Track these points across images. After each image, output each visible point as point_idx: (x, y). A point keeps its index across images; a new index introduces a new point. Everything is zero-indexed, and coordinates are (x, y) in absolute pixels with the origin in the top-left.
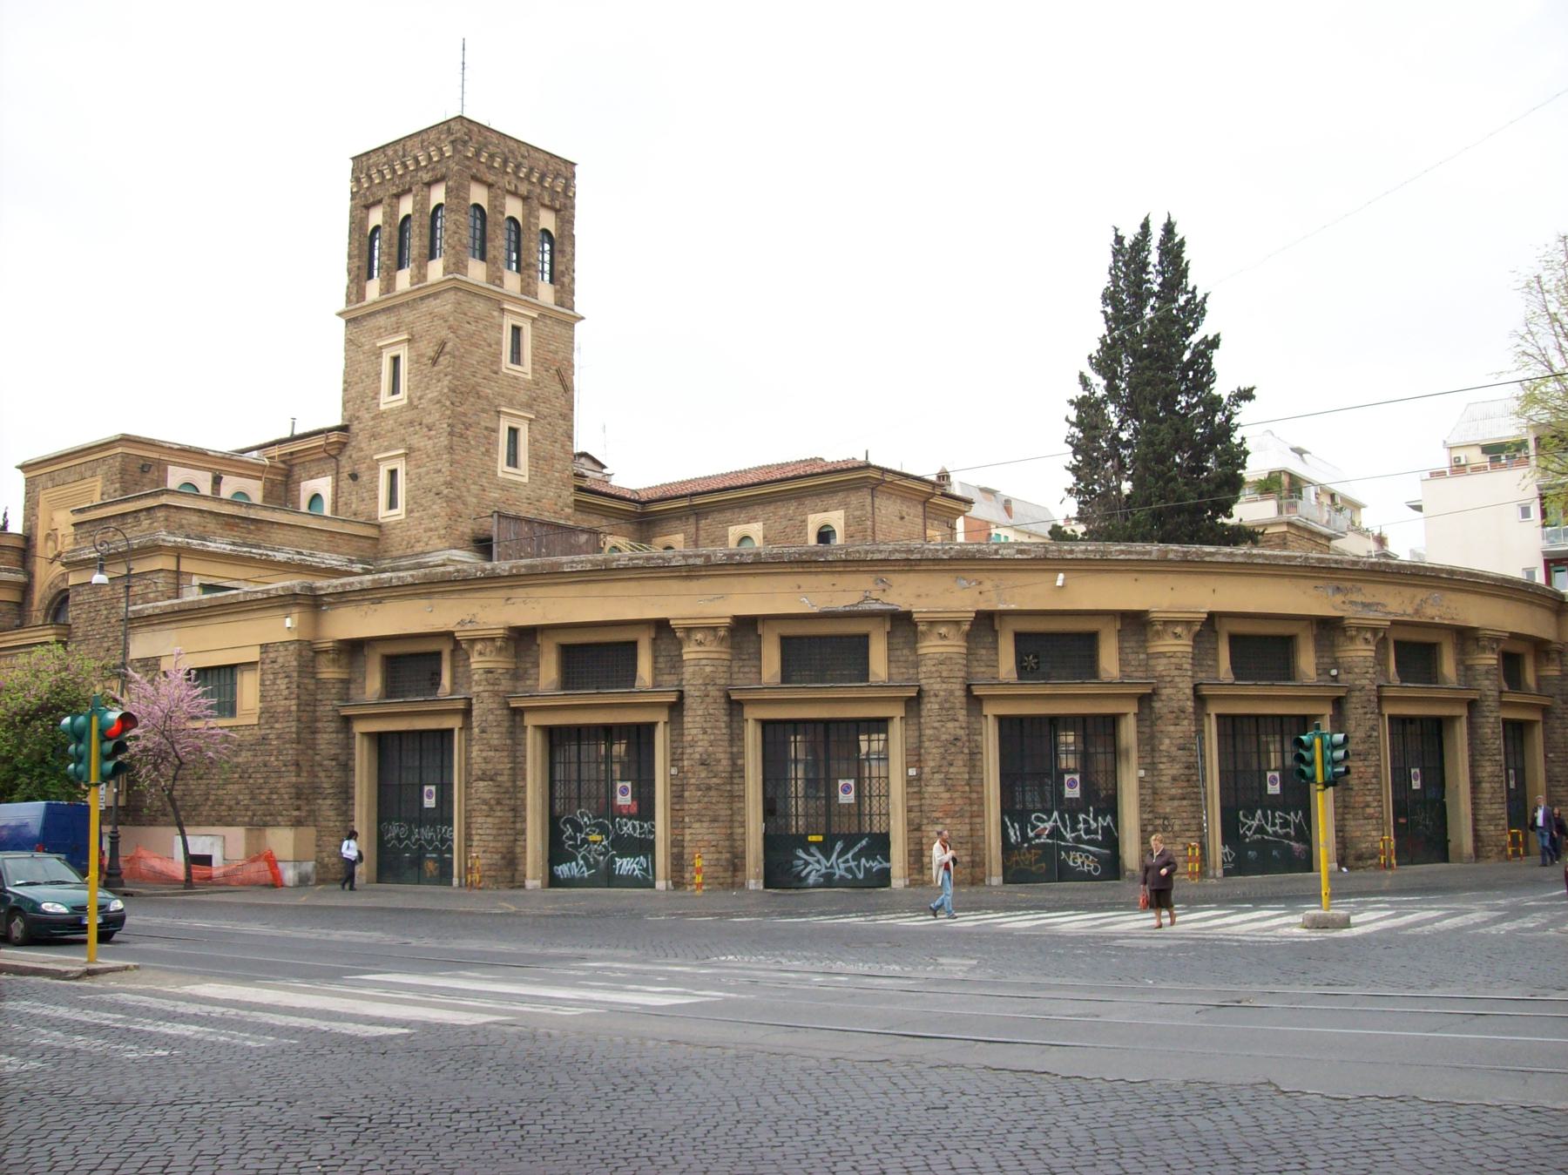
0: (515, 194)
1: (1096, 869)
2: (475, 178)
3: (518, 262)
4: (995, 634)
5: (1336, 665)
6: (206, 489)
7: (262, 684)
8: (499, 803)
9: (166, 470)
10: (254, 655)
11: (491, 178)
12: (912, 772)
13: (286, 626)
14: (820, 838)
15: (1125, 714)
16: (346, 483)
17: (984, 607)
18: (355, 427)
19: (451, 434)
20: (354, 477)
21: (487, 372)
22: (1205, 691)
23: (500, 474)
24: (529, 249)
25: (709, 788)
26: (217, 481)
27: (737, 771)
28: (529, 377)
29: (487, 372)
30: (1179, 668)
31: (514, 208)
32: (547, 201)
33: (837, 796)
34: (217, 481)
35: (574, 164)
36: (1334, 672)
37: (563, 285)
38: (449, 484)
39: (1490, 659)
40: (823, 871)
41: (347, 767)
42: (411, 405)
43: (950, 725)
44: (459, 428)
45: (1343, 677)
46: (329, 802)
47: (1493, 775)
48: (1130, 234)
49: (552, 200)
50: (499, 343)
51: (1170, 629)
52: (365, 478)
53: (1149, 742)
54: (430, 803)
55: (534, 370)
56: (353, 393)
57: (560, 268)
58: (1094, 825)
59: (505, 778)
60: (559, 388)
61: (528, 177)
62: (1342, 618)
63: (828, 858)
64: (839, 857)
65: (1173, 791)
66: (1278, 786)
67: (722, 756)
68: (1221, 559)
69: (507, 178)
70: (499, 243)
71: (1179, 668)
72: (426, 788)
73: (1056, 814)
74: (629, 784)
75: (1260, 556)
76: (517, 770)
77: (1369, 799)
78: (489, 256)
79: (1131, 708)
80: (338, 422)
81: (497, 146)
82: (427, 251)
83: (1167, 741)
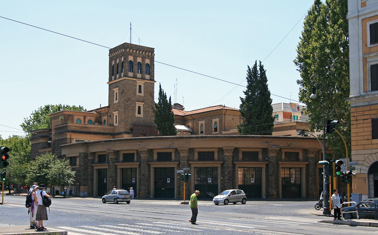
3: (141, 71)
7: (79, 159)
8: (113, 182)
10: (78, 155)
12: (178, 177)
13: (82, 150)
16: (109, 118)
18: (110, 107)
19: (125, 109)
20: (110, 116)
22: (285, 169)
23: (136, 116)
24: (143, 68)
25: (144, 179)
27: (149, 176)
30: (229, 158)
31: (139, 60)
35: (152, 50)
38: (125, 119)
39: (152, 160)
41: (93, 175)
42: (119, 103)
44: (126, 107)
45: (269, 160)
46: (90, 181)
48: (251, 67)
50: (136, 89)
52: (112, 117)
53: (223, 172)
55: (144, 94)
56: (110, 99)
57: (151, 71)
60: (151, 97)
61: (142, 53)
65: (227, 182)
69: (137, 54)
70: (136, 68)
71: (229, 158)
72: (105, 179)
76: (116, 177)
77: (273, 184)
78: (133, 71)
80: (107, 105)
81: (135, 48)
82: (112, 74)
83: (226, 172)
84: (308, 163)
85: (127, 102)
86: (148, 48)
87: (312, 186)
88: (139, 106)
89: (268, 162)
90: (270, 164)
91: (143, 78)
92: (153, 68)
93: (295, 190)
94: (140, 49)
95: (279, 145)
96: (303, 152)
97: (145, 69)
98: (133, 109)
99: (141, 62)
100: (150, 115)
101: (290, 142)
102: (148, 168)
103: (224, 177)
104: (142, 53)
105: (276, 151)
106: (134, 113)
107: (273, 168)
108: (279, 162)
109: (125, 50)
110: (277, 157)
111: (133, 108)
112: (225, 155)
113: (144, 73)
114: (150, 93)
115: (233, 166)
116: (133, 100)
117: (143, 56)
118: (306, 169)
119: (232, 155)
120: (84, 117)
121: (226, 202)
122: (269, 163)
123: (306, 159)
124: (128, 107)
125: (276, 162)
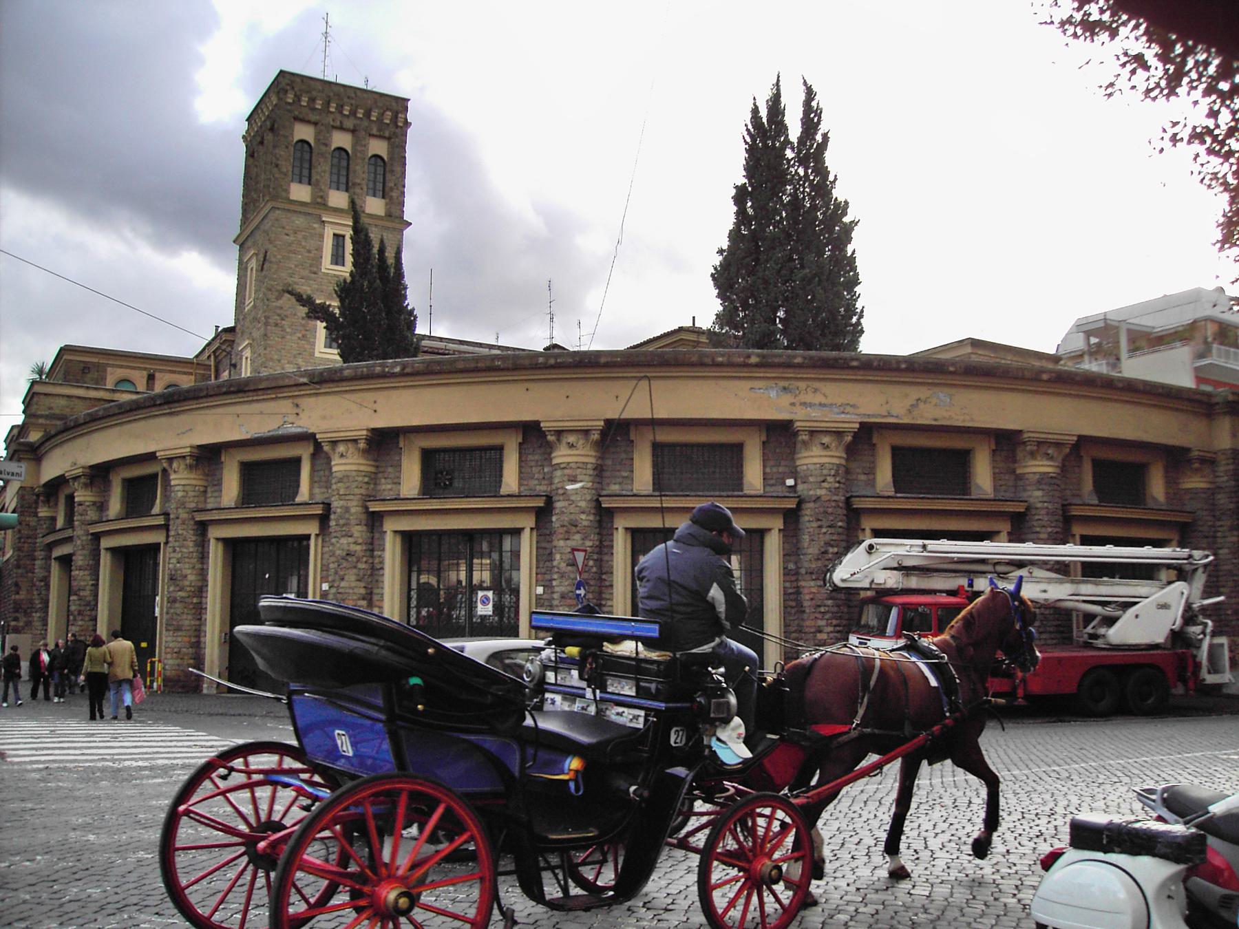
0: (341, 128)
2: (296, 119)
5: (794, 474)
6: (142, 386)
9: (105, 371)
11: (314, 118)
15: (770, 530)
19: (266, 324)
22: (858, 504)
23: (317, 355)
24: (355, 172)
26: (151, 378)
29: (306, 273)
31: (341, 140)
32: (375, 131)
34: (151, 378)
36: (790, 482)
37: (391, 198)
43: (344, 541)
45: (800, 487)
49: (379, 130)
50: (320, 249)
51: (1043, 449)
53: (544, 556)
57: (390, 184)
59: (87, 593)
61: (353, 113)
62: (791, 422)
67: (189, 572)
78: (313, 180)
79: (777, 523)
85: (277, 299)
90: (808, 511)
95: (853, 406)
97: (365, 176)
98: (303, 326)
102: (197, 544)
103: (548, 586)
106: (308, 341)
107: (824, 530)
109: (279, 99)
110: (847, 471)
112: (555, 461)
115: (600, 522)
119: (592, 460)
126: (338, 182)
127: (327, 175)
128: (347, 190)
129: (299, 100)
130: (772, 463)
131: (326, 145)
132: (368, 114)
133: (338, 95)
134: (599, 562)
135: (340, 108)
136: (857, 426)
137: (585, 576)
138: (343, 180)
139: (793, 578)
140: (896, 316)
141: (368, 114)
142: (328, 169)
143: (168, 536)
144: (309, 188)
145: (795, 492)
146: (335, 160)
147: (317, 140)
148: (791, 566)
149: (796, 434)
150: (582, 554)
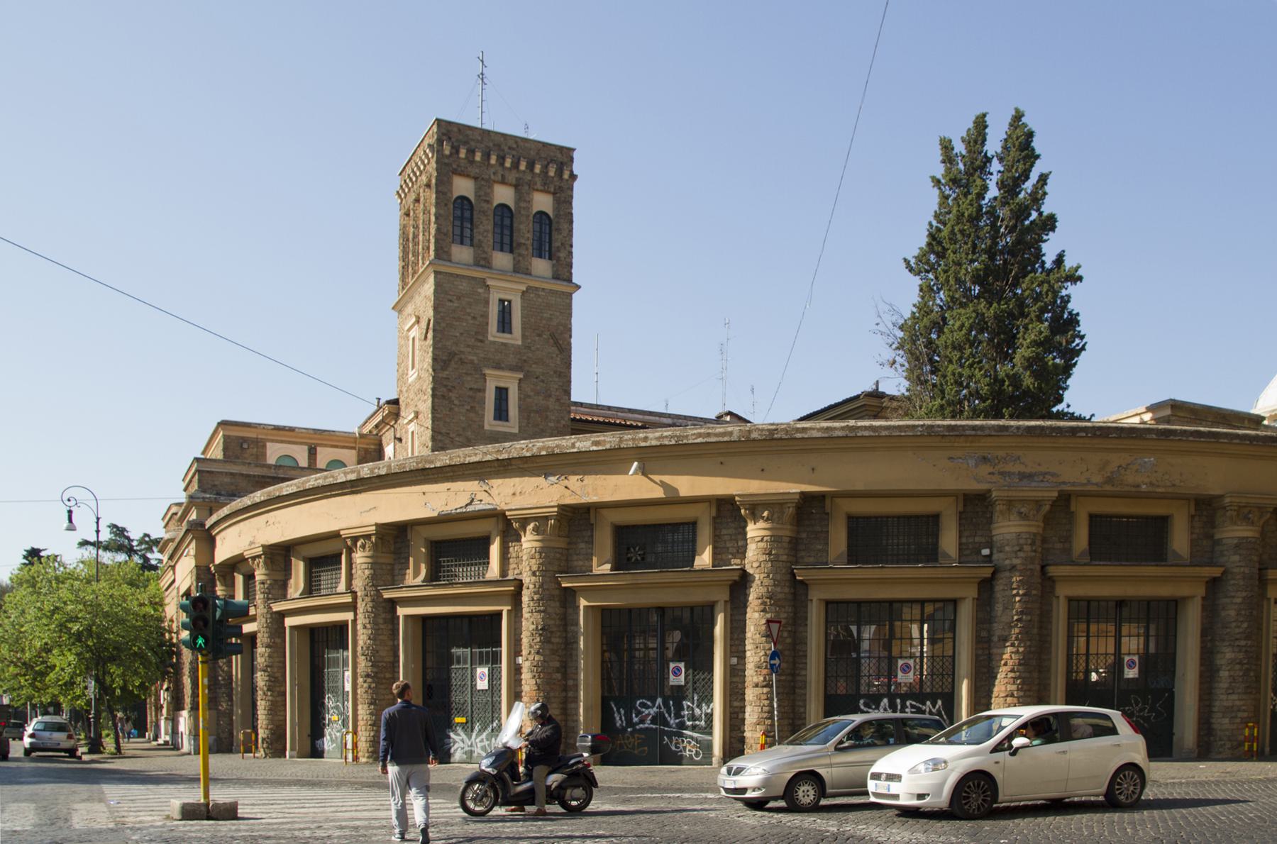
0: (503, 182)
1: (697, 754)
2: (455, 172)
4: (591, 527)
9: (264, 446)
12: (892, 740)
14: (464, 720)
15: (1192, 597)
17: (570, 500)
21: (472, 342)
23: (487, 427)
24: (519, 230)
26: (312, 453)
28: (520, 343)
31: (503, 195)
33: (896, 676)
34: (312, 453)
36: (986, 552)
37: (558, 259)
40: (467, 749)
45: (995, 557)
47: (1232, 661)
50: (485, 316)
54: (482, 684)
55: (524, 337)
57: (556, 244)
58: (697, 711)
61: (516, 165)
63: (470, 738)
64: (477, 736)
66: (1136, 670)
68: (815, 434)
69: (492, 170)
73: (659, 701)
74: (682, 665)
75: (866, 428)
78: (476, 241)
84: (1216, 572)
86: (545, 145)
87: (1231, 697)
88: (502, 385)
89: (991, 570)
91: (520, 269)
92: (565, 233)
93: (1143, 718)
94: (506, 149)
95: (1053, 475)
96: (1193, 517)
97: (530, 235)
98: (470, 397)
99: (512, 205)
100: (552, 425)
101: (1116, 460)
104: (516, 165)
105: (1038, 503)
108: (1053, 571)
110: (1044, 541)
111: (471, 393)
113: (524, 252)
114: (552, 336)
115: (794, 594)
116: (472, 362)
117: (518, 179)
118: (1204, 608)
119: (788, 533)
120: (310, 450)
121: (806, 793)
122: (994, 574)
123: (1206, 548)
124: (450, 391)
125: (1038, 568)
126: (462, 236)
127: (490, 235)
128: (511, 251)
129: (458, 152)
130: (966, 533)
131: (488, 202)
132: (531, 166)
133: (498, 146)
134: (793, 634)
135: (501, 159)
136: (1056, 494)
137: (780, 647)
138: (506, 240)
139: (986, 646)
140: (1108, 388)
141: (531, 166)
142: (490, 227)
143: (356, 615)
144: (471, 250)
145: (991, 562)
146: (498, 218)
147: (477, 196)
148: (984, 634)
149: (992, 504)
150: (777, 625)
